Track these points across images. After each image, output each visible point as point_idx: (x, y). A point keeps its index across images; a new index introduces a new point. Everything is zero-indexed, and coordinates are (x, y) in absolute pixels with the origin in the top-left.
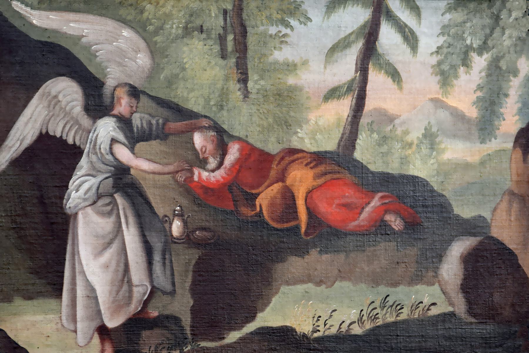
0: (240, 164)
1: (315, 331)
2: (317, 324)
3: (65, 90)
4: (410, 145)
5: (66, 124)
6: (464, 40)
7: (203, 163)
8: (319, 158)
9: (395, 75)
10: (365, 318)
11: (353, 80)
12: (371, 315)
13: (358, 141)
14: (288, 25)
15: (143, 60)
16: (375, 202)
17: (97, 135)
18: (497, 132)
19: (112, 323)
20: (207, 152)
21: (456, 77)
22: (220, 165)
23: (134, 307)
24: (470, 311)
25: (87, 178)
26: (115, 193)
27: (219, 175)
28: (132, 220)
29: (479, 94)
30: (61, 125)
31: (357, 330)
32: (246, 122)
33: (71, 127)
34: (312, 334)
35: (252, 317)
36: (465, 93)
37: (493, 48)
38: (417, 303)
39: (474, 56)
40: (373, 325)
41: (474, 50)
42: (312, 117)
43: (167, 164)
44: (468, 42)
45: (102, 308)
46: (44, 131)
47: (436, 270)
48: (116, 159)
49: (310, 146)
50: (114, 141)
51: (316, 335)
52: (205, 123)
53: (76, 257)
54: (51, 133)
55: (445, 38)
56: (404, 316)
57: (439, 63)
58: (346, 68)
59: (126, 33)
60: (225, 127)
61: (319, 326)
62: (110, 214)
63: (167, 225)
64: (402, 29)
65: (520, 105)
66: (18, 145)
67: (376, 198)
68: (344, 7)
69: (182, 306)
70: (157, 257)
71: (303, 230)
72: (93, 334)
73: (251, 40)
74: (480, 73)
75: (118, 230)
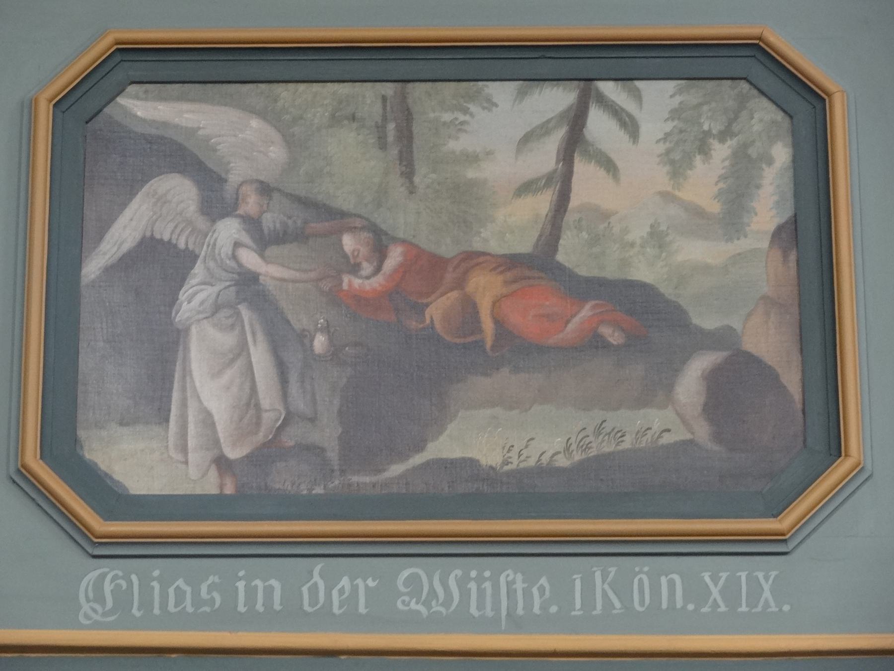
0: (404, 269)
1: (506, 462)
2: (509, 455)
3: (178, 191)
4: (632, 245)
5: (176, 227)
6: (701, 125)
7: (355, 269)
8: (511, 262)
9: (609, 165)
10: (574, 447)
11: (555, 171)
12: (581, 444)
13: (561, 241)
14: (466, 111)
15: (277, 153)
16: (586, 311)
17: (216, 240)
18: (747, 228)
19: (233, 453)
20: (360, 255)
21: (691, 167)
22: (378, 270)
23: (261, 437)
24: (717, 437)
25: (203, 287)
26: (239, 303)
27: (377, 282)
28: (260, 337)
29: (721, 185)
30: (171, 226)
31: (562, 462)
32: (413, 220)
33: (181, 231)
34: (502, 467)
35: (419, 447)
36: (704, 183)
37: (739, 133)
38: (643, 430)
39: (715, 144)
40: (584, 456)
41: (714, 136)
42: (500, 215)
43: (305, 271)
44: (706, 127)
45: (221, 435)
46: (148, 234)
47: (670, 388)
48: (240, 265)
49: (495, 247)
50: (237, 245)
51: (506, 468)
52: (358, 223)
53: (188, 378)
54: (158, 236)
55: (676, 123)
56: (627, 444)
57: (668, 152)
58: (545, 157)
59: (255, 123)
60: (383, 227)
61: (510, 458)
62: (232, 327)
63: (307, 341)
64: (616, 112)
65: (776, 198)
66: (115, 249)
67: (588, 306)
68: (540, 93)
69: (327, 434)
70: (293, 378)
71: (489, 343)
72: (210, 466)
73: (416, 128)
74: (716, 185)
75: (242, 348)
